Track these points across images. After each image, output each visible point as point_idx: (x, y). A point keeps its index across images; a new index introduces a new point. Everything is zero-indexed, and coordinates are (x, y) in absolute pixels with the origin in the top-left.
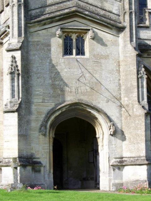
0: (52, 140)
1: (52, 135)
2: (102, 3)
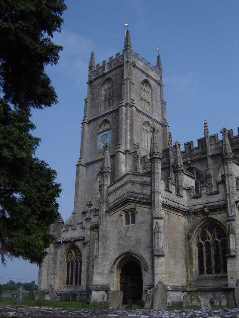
0: (119, 275)
1: (120, 272)
2: (142, 191)
